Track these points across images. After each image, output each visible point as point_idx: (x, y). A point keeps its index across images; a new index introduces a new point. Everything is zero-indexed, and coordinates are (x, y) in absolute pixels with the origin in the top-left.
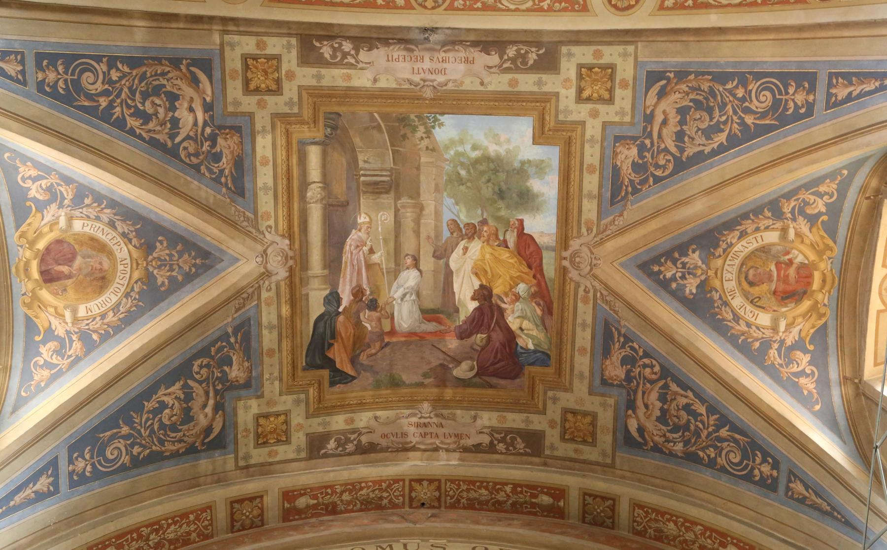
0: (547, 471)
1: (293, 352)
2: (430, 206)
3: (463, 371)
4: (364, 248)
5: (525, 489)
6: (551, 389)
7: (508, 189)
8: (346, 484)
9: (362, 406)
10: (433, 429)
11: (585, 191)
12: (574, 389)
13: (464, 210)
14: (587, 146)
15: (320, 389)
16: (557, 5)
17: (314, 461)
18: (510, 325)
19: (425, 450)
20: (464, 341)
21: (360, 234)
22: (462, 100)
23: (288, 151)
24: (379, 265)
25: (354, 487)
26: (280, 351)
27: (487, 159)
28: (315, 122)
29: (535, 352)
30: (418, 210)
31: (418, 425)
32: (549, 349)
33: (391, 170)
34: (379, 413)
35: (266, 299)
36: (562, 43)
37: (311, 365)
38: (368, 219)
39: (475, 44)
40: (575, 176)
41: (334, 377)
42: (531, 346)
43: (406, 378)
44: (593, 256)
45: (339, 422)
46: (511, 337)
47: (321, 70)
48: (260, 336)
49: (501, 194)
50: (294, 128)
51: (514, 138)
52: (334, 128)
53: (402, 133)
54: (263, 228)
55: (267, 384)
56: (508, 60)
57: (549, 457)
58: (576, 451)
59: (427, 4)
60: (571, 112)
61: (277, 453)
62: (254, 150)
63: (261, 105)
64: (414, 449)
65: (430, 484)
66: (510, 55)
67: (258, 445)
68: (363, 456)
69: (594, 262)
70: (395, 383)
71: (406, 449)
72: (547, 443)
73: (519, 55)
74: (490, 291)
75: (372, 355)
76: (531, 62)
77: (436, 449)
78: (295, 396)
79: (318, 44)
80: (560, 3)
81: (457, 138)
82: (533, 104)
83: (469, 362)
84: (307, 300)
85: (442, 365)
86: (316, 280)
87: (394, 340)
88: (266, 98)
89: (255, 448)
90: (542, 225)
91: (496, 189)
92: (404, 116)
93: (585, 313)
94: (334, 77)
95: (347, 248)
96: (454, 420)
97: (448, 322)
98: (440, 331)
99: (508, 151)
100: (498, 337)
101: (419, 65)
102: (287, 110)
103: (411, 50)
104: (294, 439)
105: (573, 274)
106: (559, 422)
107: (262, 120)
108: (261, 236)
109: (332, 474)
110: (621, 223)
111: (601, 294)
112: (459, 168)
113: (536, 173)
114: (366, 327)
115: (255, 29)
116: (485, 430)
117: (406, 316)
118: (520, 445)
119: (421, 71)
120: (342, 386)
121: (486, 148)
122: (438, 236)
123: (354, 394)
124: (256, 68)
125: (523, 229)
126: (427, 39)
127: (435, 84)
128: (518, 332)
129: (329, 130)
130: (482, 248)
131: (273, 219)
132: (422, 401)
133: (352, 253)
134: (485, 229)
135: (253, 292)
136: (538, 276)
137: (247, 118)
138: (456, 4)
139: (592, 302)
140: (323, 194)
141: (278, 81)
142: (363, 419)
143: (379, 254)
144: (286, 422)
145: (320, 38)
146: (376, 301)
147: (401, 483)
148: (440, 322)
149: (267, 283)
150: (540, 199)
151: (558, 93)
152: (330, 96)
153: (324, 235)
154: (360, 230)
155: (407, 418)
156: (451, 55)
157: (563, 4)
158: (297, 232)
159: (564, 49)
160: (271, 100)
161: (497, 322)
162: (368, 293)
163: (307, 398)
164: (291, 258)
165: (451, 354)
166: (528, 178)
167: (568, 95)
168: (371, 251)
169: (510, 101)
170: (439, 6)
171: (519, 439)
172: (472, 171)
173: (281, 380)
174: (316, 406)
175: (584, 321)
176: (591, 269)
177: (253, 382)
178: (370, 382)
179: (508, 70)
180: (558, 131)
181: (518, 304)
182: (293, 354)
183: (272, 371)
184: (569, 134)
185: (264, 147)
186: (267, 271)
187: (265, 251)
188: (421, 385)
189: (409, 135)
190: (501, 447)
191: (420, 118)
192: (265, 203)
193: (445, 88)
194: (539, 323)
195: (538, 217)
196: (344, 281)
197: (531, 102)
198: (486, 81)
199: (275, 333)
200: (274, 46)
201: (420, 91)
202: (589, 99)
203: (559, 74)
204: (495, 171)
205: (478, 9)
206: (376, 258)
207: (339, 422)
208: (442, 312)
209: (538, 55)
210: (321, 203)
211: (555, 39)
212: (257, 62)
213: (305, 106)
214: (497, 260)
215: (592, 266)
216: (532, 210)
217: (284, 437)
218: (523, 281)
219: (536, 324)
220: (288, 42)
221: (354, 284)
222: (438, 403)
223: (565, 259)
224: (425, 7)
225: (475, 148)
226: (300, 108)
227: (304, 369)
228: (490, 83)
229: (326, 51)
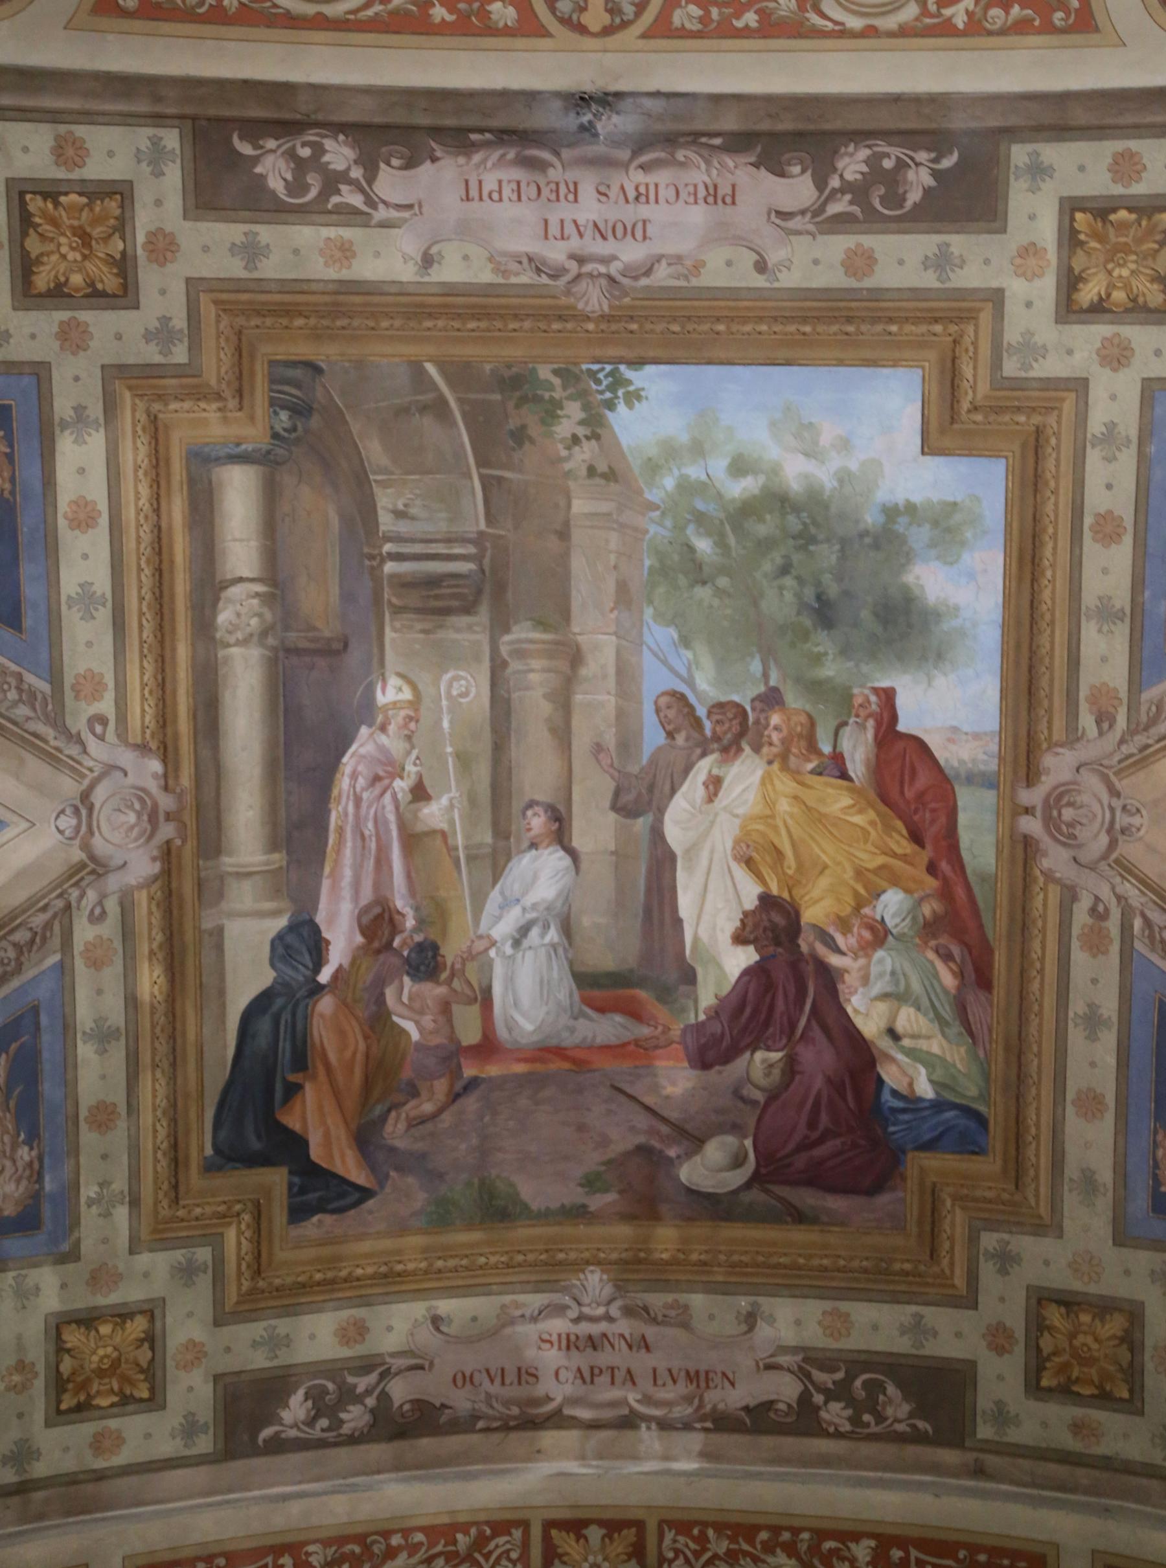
0: (984, 1495)
1: (174, 1114)
2: (602, 651)
3: (711, 1167)
4: (398, 784)
5: (914, 1553)
6: (993, 1225)
7: (846, 593)
8: (343, 1540)
9: (392, 1282)
10: (618, 1357)
11: (1089, 599)
12: (1067, 1223)
13: (707, 661)
14: (1093, 457)
15: (258, 1231)
16: (996, 12)
17: (239, 1465)
18: (858, 1022)
19: (594, 1426)
20: (712, 1075)
21: (383, 739)
22: (700, 319)
23: (156, 483)
24: (443, 834)
25: (367, 1548)
26: (132, 1108)
27: (777, 500)
28: (240, 393)
29: (938, 1105)
30: (563, 665)
31: (570, 1344)
32: (984, 1097)
33: (479, 539)
34: (445, 1306)
35: (89, 948)
36: (1011, 133)
37: (230, 1155)
38: (407, 695)
39: (737, 143)
40: (1055, 553)
41: (303, 1191)
42: (925, 1089)
43: (535, 1191)
44: (1117, 804)
45: (317, 1336)
46: (859, 1059)
48: (68, 1065)
49: (824, 612)
50: (176, 411)
51: (864, 434)
52: (300, 410)
53: (512, 424)
54: (78, 723)
55: (89, 1217)
56: (842, 191)
57: (988, 1447)
58: (1077, 1428)
59: (586, 19)
60: (1042, 352)
61: (119, 1440)
62: (49, 481)
63: (72, 338)
64: (557, 1420)
65: (609, 1536)
66: (849, 176)
67: (58, 1416)
68: (397, 1445)
69: (1122, 820)
70: (496, 1209)
71: (531, 1420)
72: (984, 1402)
73: (875, 173)
74: (792, 914)
75: (423, 1120)
76: (914, 197)
77: (629, 1422)
78: (179, 1255)
79: (246, 149)
80: (1007, 8)
81: (684, 438)
82: (923, 328)
83: (730, 1140)
84: (219, 948)
85: (643, 1150)
86: (247, 885)
87: (493, 1070)
88: (85, 316)
89: (49, 1424)
90: (953, 706)
91: (809, 593)
92: (519, 367)
93: (1095, 981)
94: (299, 251)
95: (343, 783)
96: (685, 1325)
97: (661, 1012)
98: (637, 1043)
99: (844, 477)
100: (819, 1059)
101: (564, 211)
102: (152, 354)
103: (537, 165)
104: (175, 1395)
105: (1055, 859)
106: (1020, 1334)
107: (74, 386)
108: (74, 750)
109: (295, 1508)
111: (1147, 922)
112: (690, 530)
113: (932, 544)
114: (403, 1032)
115: (48, 102)
116: (783, 1360)
117: (528, 996)
118: (898, 1408)
119: (570, 229)
120: (328, 1219)
121: (775, 470)
122: (628, 743)
123: (366, 1246)
124: (54, 222)
125: (894, 718)
126: (588, 130)
127: (614, 269)
128: (885, 1044)
129: (284, 415)
130: (766, 780)
131: (110, 695)
132: (579, 1266)
133: (358, 801)
134: (775, 719)
135: (48, 925)
136: (944, 866)
137: (26, 380)
138: (678, 18)
139: (1115, 948)
140: (268, 616)
141: (124, 266)
142: (397, 1325)
143: (444, 801)
144: (150, 1339)
145: (255, 130)
146: (435, 948)
147: (517, 1534)
148: (635, 1013)
149: (91, 895)
150: (945, 626)
151: (1000, 292)
152: (288, 311)
153: (271, 745)
154: (383, 729)
155: (534, 1319)
156: (663, 177)
157: (1016, 10)
158: (185, 734)
159: (1019, 154)
160: (102, 323)
161: (814, 1011)
162: (410, 923)
163: (219, 1261)
164: (168, 817)
165: (674, 1115)
166: (907, 557)
167: (1031, 298)
168: (420, 793)
169: (849, 320)
170: (625, 24)
171: (891, 1389)
172: (732, 540)
173: (134, 1202)
174: (246, 1285)
175: (1092, 1007)
176: (1113, 844)
177: (47, 1211)
178: (418, 1205)
179: (842, 223)
180: (998, 410)
181: (880, 954)
182: (174, 1121)
183: (106, 1173)
184: (1036, 419)
185: (81, 471)
186: (92, 858)
187: (85, 796)
188: (577, 1213)
189: (534, 430)
190: (835, 1413)
191: (567, 375)
192: (87, 645)
193: (644, 282)
194: (947, 1012)
195: (940, 681)
196: (335, 887)
197: (917, 321)
198: (772, 258)
199: (118, 1053)
200: (111, 154)
201: (568, 293)
202: (1099, 309)
203: (1003, 230)
204: (806, 540)
205: (745, 33)
206: (433, 814)
207: (317, 1336)
208: (642, 983)
209: (935, 174)
210: (261, 643)
211: (993, 122)
212: (57, 204)
213: (209, 341)
214: (815, 817)
215: (1116, 833)
216: (924, 658)
217: (141, 1385)
218: (895, 881)
219: (938, 1017)
220: (156, 142)
221: (367, 896)
222: (634, 1270)
223: (1028, 811)
224: (582, 29)
225: (740, 467)
226: (195, 346)
227: (209, 1167)
228: (787, 265)
229: (274, 171)
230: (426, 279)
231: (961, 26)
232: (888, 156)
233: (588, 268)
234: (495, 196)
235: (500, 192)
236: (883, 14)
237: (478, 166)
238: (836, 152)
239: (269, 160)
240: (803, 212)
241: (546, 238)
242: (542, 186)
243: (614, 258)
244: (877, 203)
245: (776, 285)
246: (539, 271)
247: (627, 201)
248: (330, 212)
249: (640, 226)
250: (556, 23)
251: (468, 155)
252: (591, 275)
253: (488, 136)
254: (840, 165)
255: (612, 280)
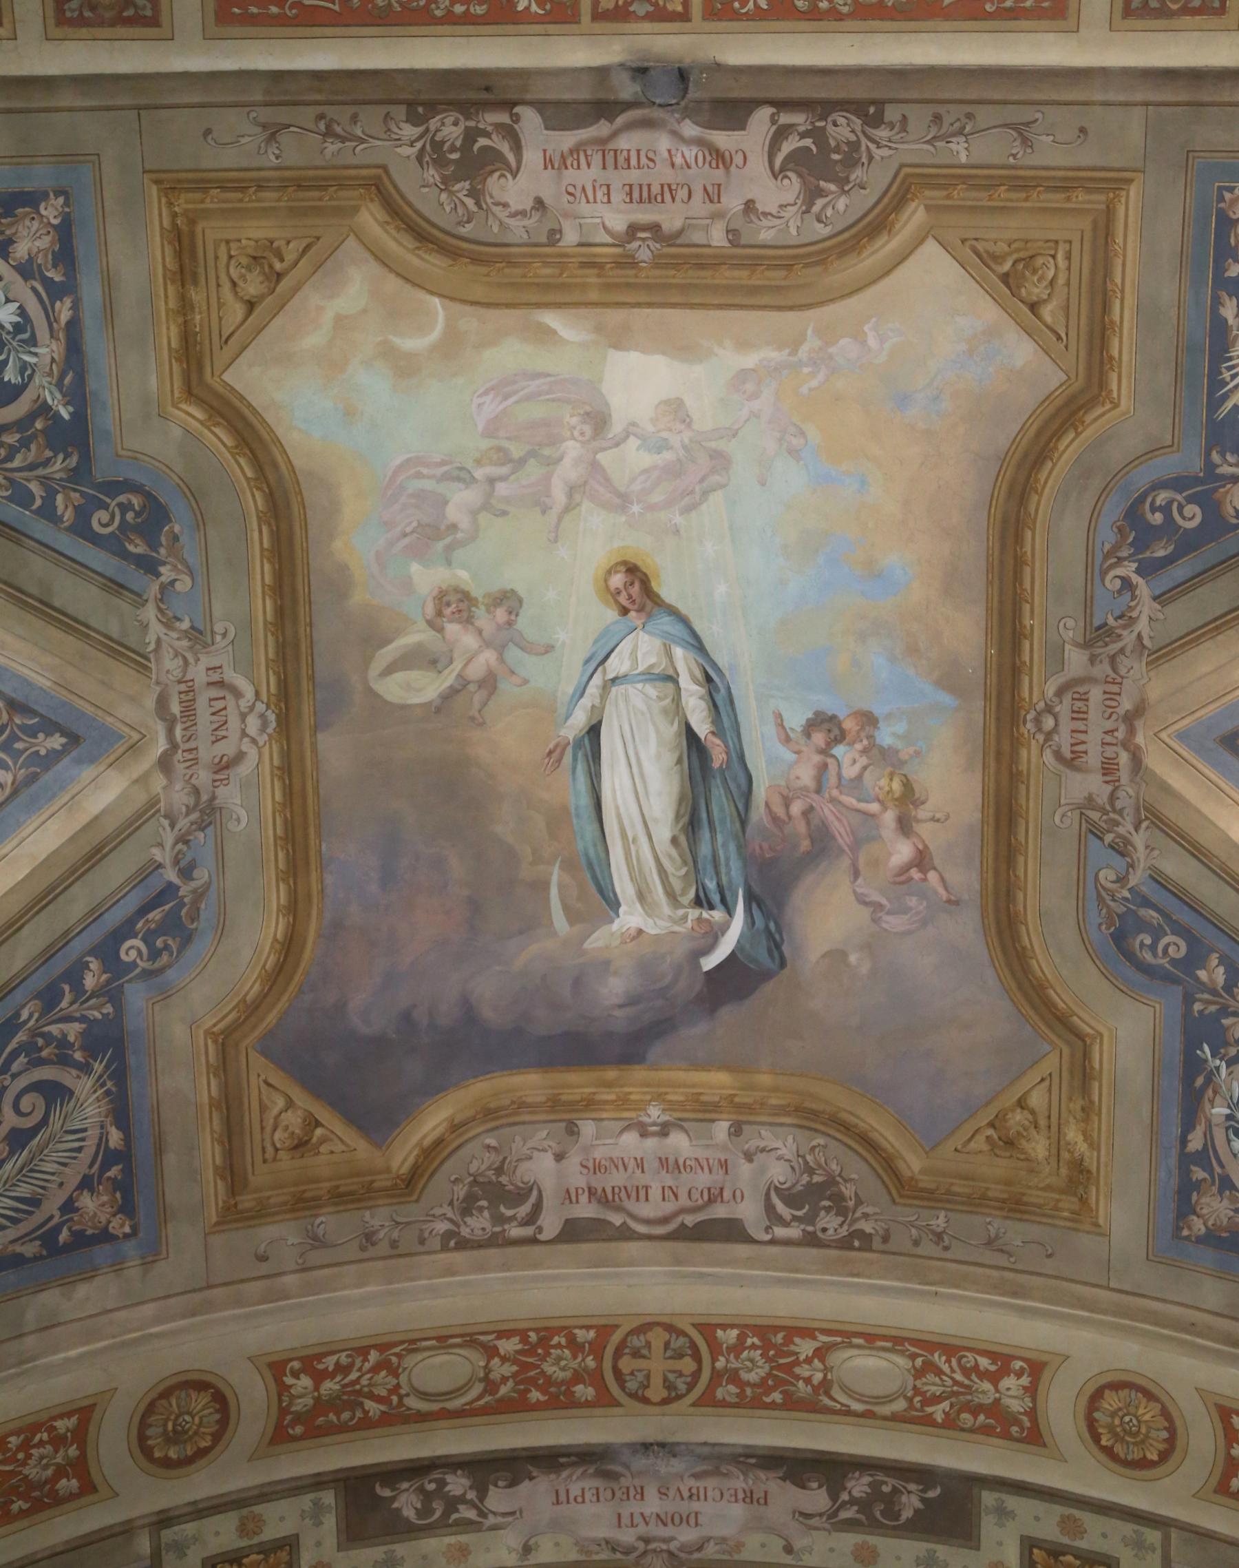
47: (396, 1547)
59: (649, 1393)
66: (856, 1493)
76: (907, 1514)
79: (387, 1493)
101: (634, 1507)
110: (1070, 623)
127: (673, 1546)
138: (719, 1393)
156: (711, 1483)
170: (679, 1397)
193: (696, 1556)
198: (798, 1544)
200: (282, 1519)
203: (978, 1549)
205: (773, 1406)
209: (923, 1500)
220: (316, 1503)
229: (407, 1503)
230: (526, 1563)
231: (940, 1421)
232: (886, 1483)
233: (653, 1546)
234: (580, 1499)
235: (583, 1496)
236: (877, 1404)
237: (566, 1479)
238: (845, 1476)
239: (403, 1498)
240: (821, 1515)
241: (620, 1526)
242: (616, 1490)
243: (672, 1539)
244: (878, 1514)
245: (800, 1563)
246: (614, 1550)
247: (682, 1499)
248: (450, 1526)
249: (693, 1515)
250: (627, 1398)
251: (558, 1473)
252: (654, 1551)
253: (573, 1458)
254: (849, 1485)
255: (670, 1553)
